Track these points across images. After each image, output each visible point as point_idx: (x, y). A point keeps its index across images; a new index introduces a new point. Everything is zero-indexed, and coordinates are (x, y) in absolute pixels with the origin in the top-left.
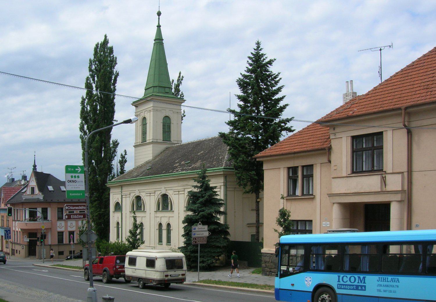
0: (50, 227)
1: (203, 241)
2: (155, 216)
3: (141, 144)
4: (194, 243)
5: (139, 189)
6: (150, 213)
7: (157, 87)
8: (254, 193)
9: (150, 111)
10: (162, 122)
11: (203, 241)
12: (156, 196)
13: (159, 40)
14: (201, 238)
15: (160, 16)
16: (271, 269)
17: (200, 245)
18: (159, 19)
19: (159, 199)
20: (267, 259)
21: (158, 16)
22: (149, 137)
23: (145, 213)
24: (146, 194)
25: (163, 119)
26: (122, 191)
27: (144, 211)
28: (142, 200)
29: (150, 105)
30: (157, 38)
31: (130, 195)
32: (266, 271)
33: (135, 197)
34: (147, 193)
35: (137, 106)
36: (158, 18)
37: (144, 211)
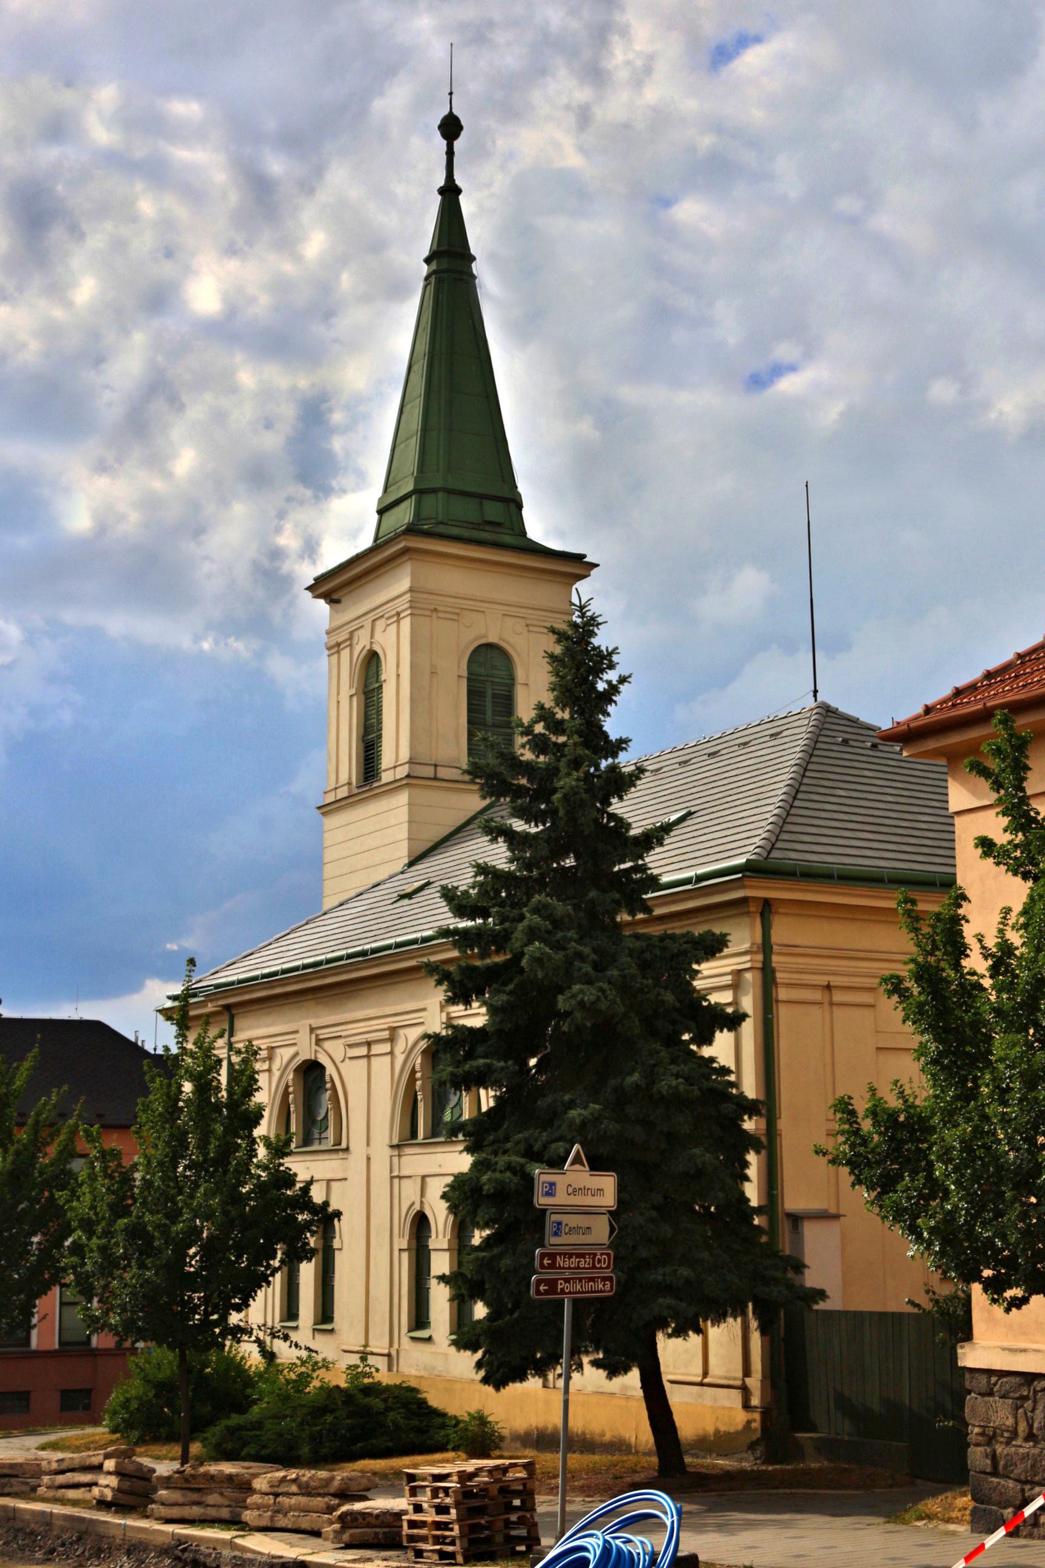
0: (88, 1387)
1: (592, 1279)
2: (395, 1174)
3: (356, 791)
4: (542, 1288)
5: (315, 1023)
6: (369, 1159)
7: (440, 494)
8: (613, 736)
9: (398, 614)
10: (465, 674)
11: (592, 1279)
12: (400, 1059)
13: (450, 254)
14: (582, 1256)
15: (458, 144)
16: (1026, 1482)
17: (575, 1303)
18: (450, 153)
19: (413, 1072)
20: (1001, 1414)
21: (445, 142)
22: (394, 752)
23: (341, 1155)
24: (350, 1046)
25: (471, 661)
26: (233, 1039)
27: (340, 1149)
28: (328, 1086)
29: (398, 584)
30: (442, 249)
31: (392, 1039)
32: (995, 1497)
33: (296, 1070)
34: (352, 1040)
35: (335, 596)
36: (445, 149)
37: (340, 1149)
